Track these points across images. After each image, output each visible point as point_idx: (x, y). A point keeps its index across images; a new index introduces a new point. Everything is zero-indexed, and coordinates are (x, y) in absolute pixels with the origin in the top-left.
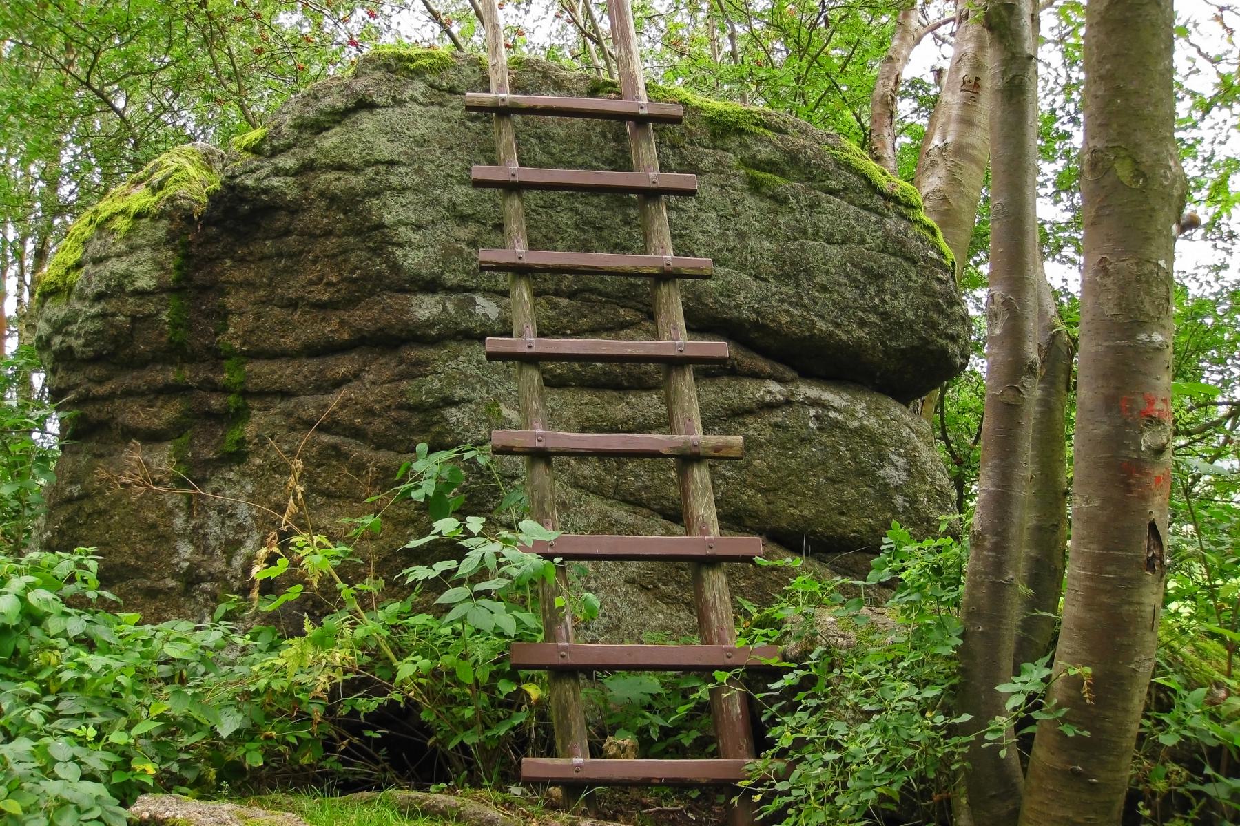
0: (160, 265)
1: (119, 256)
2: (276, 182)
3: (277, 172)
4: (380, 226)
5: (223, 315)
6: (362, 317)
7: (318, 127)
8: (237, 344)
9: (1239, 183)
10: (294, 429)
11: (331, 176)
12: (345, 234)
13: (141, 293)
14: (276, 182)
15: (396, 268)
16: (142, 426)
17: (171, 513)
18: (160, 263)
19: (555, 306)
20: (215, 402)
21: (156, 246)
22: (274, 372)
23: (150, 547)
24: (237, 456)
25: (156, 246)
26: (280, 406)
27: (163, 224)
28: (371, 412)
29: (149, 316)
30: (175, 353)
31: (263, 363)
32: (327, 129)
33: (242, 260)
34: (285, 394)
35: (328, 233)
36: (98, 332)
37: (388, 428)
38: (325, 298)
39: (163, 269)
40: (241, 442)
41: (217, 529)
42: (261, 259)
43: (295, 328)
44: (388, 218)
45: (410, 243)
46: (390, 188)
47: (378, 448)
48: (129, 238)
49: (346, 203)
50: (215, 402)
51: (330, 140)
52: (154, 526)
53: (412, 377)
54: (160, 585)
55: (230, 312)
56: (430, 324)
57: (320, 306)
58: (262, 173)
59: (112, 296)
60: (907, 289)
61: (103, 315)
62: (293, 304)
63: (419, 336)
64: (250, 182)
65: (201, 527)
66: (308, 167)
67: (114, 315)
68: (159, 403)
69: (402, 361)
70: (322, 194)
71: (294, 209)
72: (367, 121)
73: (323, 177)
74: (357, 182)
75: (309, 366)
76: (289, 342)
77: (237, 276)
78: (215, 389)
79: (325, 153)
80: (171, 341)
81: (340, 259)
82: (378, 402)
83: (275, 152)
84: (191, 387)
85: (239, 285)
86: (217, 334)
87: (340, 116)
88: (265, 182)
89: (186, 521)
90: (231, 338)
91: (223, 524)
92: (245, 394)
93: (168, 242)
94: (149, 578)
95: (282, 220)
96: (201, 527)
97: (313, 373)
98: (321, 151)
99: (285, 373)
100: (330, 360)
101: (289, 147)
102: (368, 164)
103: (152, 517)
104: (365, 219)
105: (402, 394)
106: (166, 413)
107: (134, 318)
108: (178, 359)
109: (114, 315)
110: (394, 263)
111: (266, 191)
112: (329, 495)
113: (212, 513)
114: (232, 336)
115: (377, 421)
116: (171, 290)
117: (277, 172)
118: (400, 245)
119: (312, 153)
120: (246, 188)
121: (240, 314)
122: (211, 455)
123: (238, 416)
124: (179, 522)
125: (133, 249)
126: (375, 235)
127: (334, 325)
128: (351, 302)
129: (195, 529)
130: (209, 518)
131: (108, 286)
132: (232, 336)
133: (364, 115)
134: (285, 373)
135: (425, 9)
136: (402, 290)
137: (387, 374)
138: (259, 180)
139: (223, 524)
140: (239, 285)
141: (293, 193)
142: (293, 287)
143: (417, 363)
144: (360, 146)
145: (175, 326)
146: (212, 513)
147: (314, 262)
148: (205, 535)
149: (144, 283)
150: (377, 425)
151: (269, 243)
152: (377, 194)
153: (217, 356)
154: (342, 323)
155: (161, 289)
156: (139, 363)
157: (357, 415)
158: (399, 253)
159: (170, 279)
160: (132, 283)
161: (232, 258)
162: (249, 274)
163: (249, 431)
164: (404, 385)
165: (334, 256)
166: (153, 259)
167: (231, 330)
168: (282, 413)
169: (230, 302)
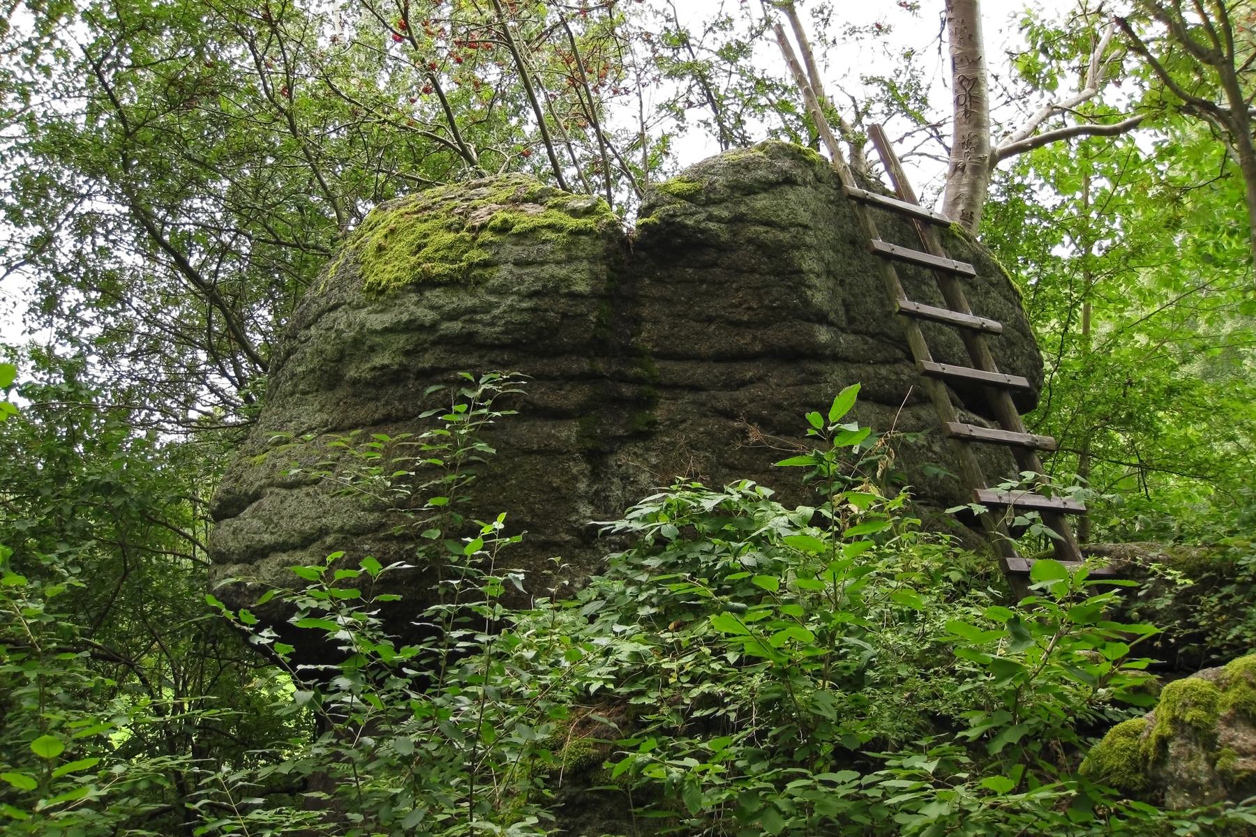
0: (594, 276)
1: (558, 263)
2: (712, 225)
3: (710, 218)
4: (801, 271)
5: (637, 321)
6: (778, 335)
7: (750, 191)
8: (649, 346)
9: (3, 270)
10: (705, 416)
11: (761, 229)
12: (769, 273)
13: (574, 296)
14: (712, 225)
15: (806, 302)
16: (552, 405)
17: (575, 478)
18: (595, 274)
19: (866, 343)
20: (626, 390)
21: (593, 259)
22: (687, 371)
23: (549, 507)
24: (643, 435)
25: (593, 259)
26: (688, 397)
27: (601, 243)
28: (779, 407)
29: (582, 315)
30: (598, 347)
31: (673, 363)
32: (755, 193)
33: (660, 281)
34: (694, 388)
35: (753, 271)
36: (526, 323)
37: (794, 419)
38: (745, 318)
39: (597, 278)
40: (653, 423)
41: (619, 492)
42: (679, 282)
43: (710, 338)
44: (805, 267)
45: (815, 287)
46: (805, 245)
47: (777, 434)
48: (568, 250)
49: (773, 251)
50: (626, 390)
51: (762, 202)
52: (558, 489)
53: (810, 383)
54: (557, 538)
55: (644, 320)
56: (825, 346)
57: (737, 324)
58: (697, 217)
59: (546, 294)
60: (1022, 353)
61: (533, 310)
62: (710, 320)
63: (817, 354)
64: (690, 222)
65: (604, 490)
66: (739, 219)
67: (546, 310)
68: (568, 387)
69: (803, 371)
70: (750, 241)
71: (722, 248)
72: (791, 195)
73: (753, 229)
74: (785, 237)
75: (718, 369)
76: (703, 348)
77: (655, 292)
78: (623, 379)
79: (757, 211)
80: (594, 337)
81: (762, 291)
82: (786, 399)
83: (709, 202)
84: (603, 376)
85: (654, 300)
86: (632, 336)
87: (768, 186)
88: (703, 225)
89: (588, 486)
90: (644, 340)
91: (624, 488)
92: (659, 386)
93: (604, 258)
94: (543, 533)
95: (711, 255)
96: (604, 490)
97: (722, 374)
98: (753, 209)
99: (698, 372)
100: (737, 366)
101: (721, 201)
102: (792, 225)
103: (556, 482)
104: (789, 265)
105: (807, 395)
106: (575, 396)
107: (564, 315)
108: (592, 353)
109: (546, 310)
110: (806, 300)
111: (703, 231)
112: (732, 467)
113: (615, 480)
114: (645, 338)
115: (782, 414)
116: (601, 297)
117: (710, 218)
118: (810, 287)
119: (743, 209)
120: (686, 226)
121: (654, 323)
122: (621, 432)
123: (646, 403)
124: (582, 486)
125: (570, 260)
126: (793, 276)
127: (748, 338)
128: (765, 324)
129: (597, 493)
130: (612, 483)
131: (544, 286)
132: (645, 338)
133: (787, 188)
134: (698, 372)
135: (638, 115)
136: (809, 320)
137: (790, 380)
138: (699, 222)
139: (624, 488)
140: (654, 300)
141: (725, 237)
142: (715, 306)
143: (817, 374)
144: (787, 211)
145: (599, 323)
146: (615, 480)
147: (737, 290)
148: (607, 498)
149: (581, 288)
150: (782, 416)
151: (690, 271)
152: (798, 248)
153: (632, 354)
154: (755, 338)
155: (594, 294)
156: (557, 352)
157: (764, 408)
158: (809, 293)
159: (602, 288)
160: (568, 286)
161: (650, 278)
162: (668, 291)
163: (659, 414)
164: (806, 389)
165: (758, 288)
166: (591, 270)
167: (644, 334)
168: (693, 402)
169: (645, 312)
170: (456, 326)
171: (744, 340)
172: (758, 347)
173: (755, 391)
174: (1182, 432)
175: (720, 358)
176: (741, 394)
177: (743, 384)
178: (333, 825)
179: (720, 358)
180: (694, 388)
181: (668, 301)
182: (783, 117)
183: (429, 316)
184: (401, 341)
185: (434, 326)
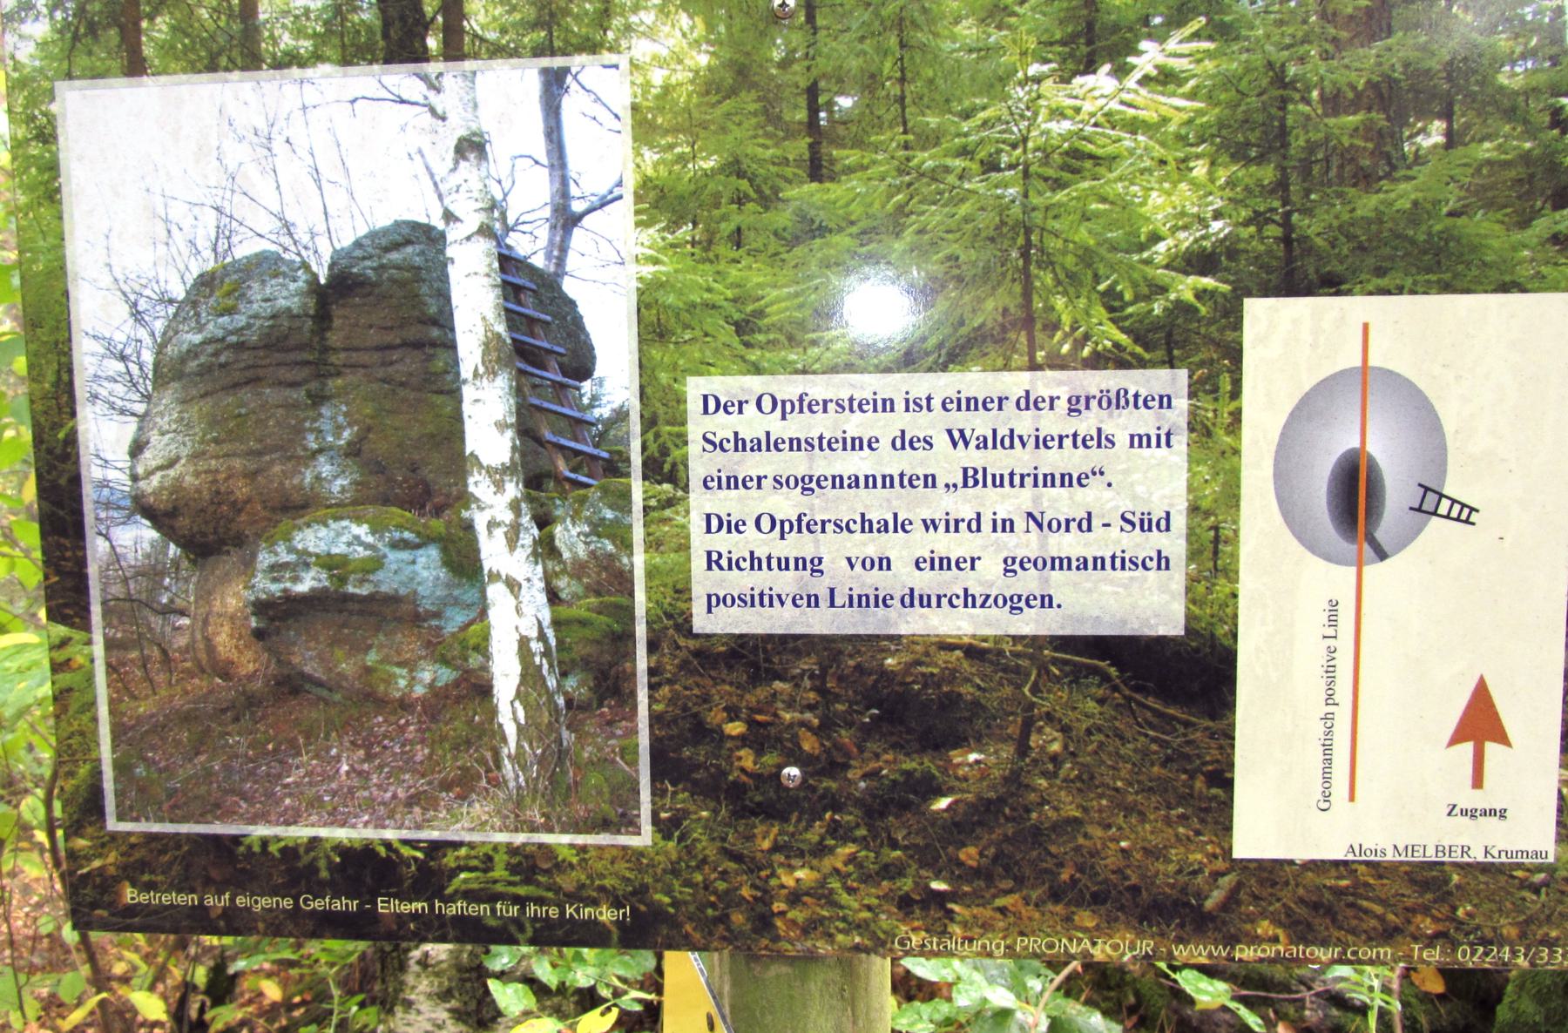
6: (413, 333)
15: (424, 314)
26: (362, 371)
66: (382, 267)
71: (374, 285)
95: (368, 289)
99: (364, 358)
134: (364, 358)
170: (234, 339)
171: (389, 338)
172: (398, 341)
173: (397, 367)
174: (387, 550)
175: (379, 348)
176: (390, 369)
177: (392, 363)
178: (1365, 903)
179: (379, 348)
180: (364, 366)
181: (346, 317)
182: (436, 13)
183: (220, 333)
184: (210, 349)
185: (223, 339)
